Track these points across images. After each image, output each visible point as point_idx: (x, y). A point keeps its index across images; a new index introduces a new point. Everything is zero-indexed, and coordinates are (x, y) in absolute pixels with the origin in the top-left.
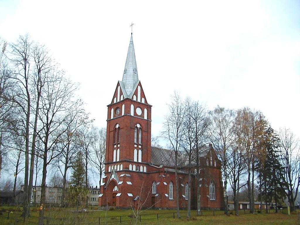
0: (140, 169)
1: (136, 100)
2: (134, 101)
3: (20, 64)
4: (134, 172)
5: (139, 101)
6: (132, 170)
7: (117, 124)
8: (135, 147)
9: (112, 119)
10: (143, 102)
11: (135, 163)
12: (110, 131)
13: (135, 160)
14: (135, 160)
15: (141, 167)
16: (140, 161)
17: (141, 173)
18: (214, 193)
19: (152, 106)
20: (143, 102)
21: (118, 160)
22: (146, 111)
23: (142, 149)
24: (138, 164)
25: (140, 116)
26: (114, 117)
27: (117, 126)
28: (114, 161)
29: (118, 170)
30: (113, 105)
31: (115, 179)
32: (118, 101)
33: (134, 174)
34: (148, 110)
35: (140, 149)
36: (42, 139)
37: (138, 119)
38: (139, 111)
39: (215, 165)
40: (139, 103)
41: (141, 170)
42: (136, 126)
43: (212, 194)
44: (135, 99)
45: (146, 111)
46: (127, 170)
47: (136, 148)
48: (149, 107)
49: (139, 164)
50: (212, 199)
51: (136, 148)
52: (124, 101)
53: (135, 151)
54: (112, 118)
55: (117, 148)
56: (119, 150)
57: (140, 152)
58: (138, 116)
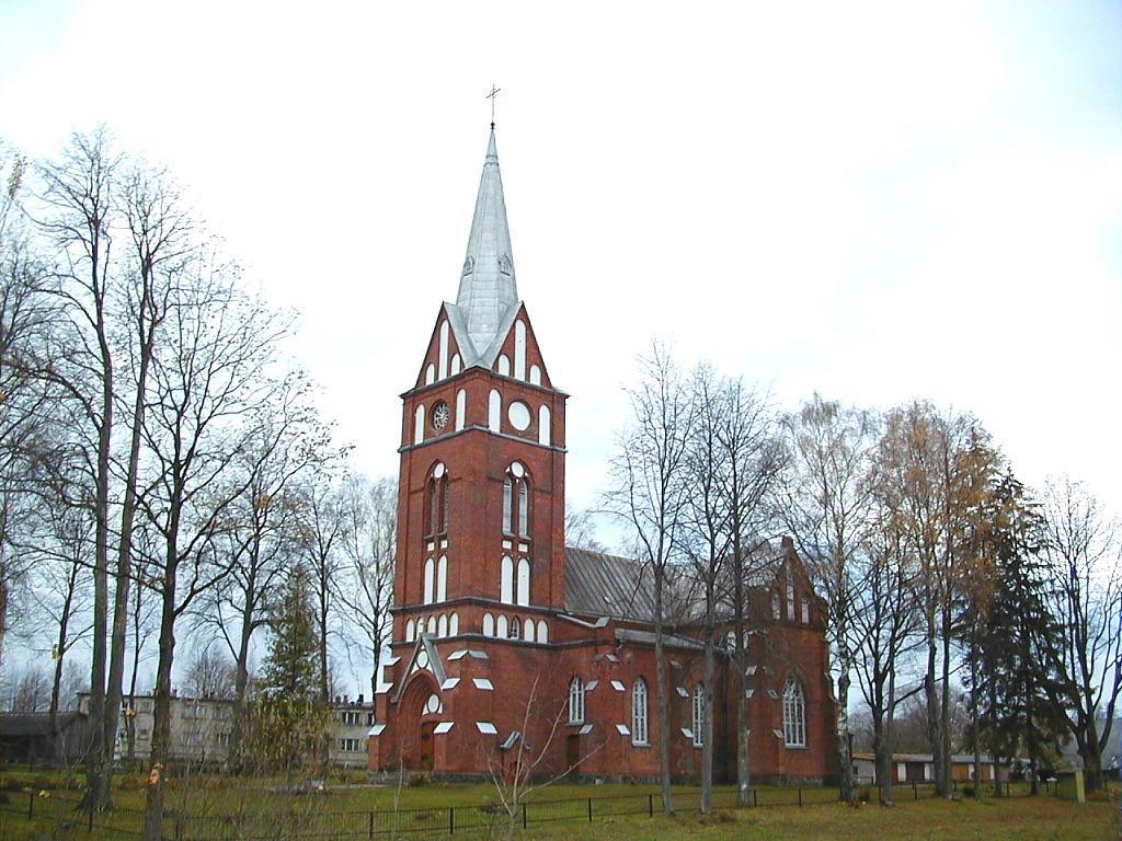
0: (522, 632)
1: (507, 374)
2: (502, 379)
3: (77, 238)
4: (501, 642)
5: (520, 376)
6: (495, 634)
7: (437, 462)
8: (504, 550)
9: (420, 446)
10: (535, 380)
11: (505, 607)
12: (413, 488)
13: (506, 599)
14: (506, 599)
15: (529, 625)
16: (523, 601)
17: (528, 645)
18: (800, 721)
19: (568, 397)
20: (535, 380)
21: (441, 599)
22: (544, 413)
23: (530, 558)
24: (515, 614)
25: (524, 434)
26: (426, 436)
27: (439, 472)
28: (428, 600)
29: (442, 635)
30: (423, 392)
31: (429, 668)
32: (443, 376)
33: (502, 652)
34: (552, 412)
35: (523, 555)
36: (158, 520)
37: (518, 444)
38: (519, 417)
39: (805, 617)
40: (519, 384)
41: (529, 637)
42: (508, 470)
43: (794, 726)
44: (504, 370)
45: (544, 413)
46: (476, 635)
47: (507, 553)
48: (557, 401)
49: (519, 615)
50: (791, 744)
51: (507, 553)
52: (464, 377)
53: (507, 564)
54: (419, 440)
55: (439, 553)
56: (444, 559)
57: (524, 567)
58: (517, 435)
